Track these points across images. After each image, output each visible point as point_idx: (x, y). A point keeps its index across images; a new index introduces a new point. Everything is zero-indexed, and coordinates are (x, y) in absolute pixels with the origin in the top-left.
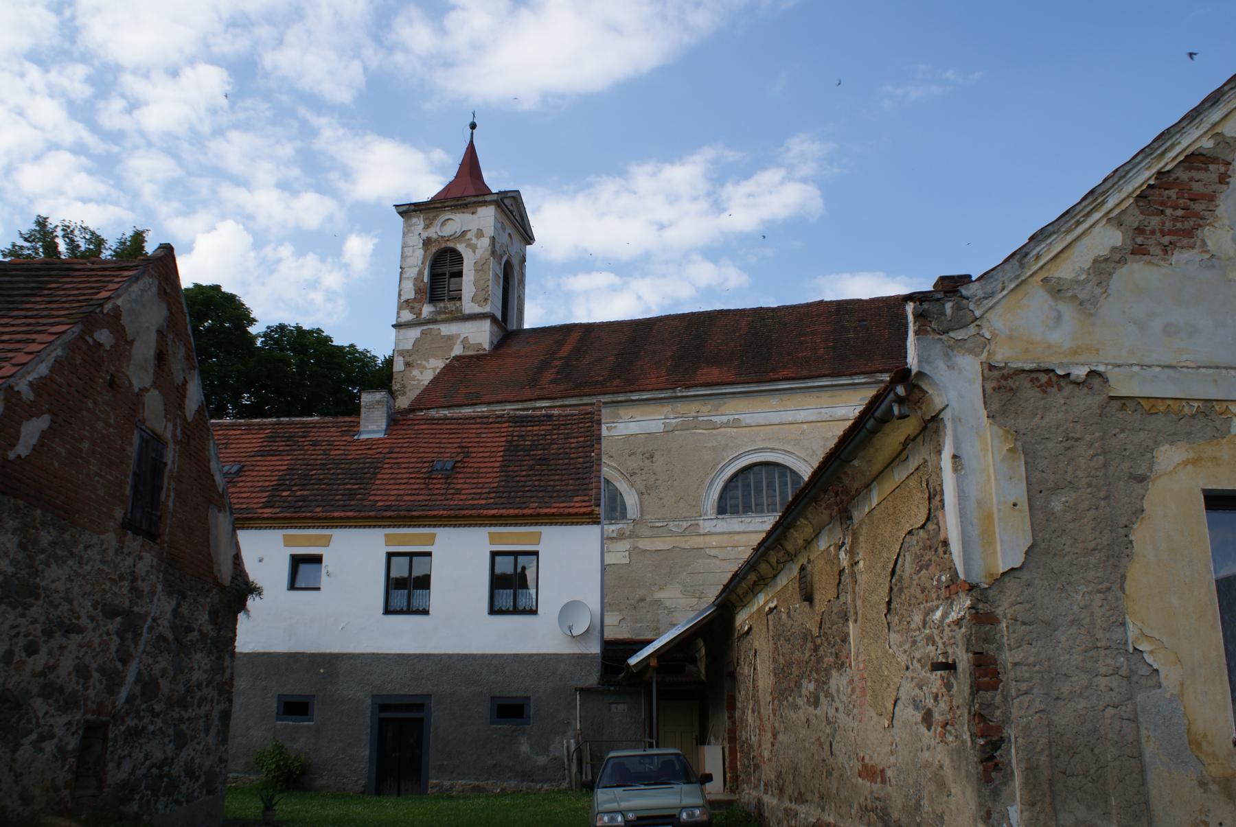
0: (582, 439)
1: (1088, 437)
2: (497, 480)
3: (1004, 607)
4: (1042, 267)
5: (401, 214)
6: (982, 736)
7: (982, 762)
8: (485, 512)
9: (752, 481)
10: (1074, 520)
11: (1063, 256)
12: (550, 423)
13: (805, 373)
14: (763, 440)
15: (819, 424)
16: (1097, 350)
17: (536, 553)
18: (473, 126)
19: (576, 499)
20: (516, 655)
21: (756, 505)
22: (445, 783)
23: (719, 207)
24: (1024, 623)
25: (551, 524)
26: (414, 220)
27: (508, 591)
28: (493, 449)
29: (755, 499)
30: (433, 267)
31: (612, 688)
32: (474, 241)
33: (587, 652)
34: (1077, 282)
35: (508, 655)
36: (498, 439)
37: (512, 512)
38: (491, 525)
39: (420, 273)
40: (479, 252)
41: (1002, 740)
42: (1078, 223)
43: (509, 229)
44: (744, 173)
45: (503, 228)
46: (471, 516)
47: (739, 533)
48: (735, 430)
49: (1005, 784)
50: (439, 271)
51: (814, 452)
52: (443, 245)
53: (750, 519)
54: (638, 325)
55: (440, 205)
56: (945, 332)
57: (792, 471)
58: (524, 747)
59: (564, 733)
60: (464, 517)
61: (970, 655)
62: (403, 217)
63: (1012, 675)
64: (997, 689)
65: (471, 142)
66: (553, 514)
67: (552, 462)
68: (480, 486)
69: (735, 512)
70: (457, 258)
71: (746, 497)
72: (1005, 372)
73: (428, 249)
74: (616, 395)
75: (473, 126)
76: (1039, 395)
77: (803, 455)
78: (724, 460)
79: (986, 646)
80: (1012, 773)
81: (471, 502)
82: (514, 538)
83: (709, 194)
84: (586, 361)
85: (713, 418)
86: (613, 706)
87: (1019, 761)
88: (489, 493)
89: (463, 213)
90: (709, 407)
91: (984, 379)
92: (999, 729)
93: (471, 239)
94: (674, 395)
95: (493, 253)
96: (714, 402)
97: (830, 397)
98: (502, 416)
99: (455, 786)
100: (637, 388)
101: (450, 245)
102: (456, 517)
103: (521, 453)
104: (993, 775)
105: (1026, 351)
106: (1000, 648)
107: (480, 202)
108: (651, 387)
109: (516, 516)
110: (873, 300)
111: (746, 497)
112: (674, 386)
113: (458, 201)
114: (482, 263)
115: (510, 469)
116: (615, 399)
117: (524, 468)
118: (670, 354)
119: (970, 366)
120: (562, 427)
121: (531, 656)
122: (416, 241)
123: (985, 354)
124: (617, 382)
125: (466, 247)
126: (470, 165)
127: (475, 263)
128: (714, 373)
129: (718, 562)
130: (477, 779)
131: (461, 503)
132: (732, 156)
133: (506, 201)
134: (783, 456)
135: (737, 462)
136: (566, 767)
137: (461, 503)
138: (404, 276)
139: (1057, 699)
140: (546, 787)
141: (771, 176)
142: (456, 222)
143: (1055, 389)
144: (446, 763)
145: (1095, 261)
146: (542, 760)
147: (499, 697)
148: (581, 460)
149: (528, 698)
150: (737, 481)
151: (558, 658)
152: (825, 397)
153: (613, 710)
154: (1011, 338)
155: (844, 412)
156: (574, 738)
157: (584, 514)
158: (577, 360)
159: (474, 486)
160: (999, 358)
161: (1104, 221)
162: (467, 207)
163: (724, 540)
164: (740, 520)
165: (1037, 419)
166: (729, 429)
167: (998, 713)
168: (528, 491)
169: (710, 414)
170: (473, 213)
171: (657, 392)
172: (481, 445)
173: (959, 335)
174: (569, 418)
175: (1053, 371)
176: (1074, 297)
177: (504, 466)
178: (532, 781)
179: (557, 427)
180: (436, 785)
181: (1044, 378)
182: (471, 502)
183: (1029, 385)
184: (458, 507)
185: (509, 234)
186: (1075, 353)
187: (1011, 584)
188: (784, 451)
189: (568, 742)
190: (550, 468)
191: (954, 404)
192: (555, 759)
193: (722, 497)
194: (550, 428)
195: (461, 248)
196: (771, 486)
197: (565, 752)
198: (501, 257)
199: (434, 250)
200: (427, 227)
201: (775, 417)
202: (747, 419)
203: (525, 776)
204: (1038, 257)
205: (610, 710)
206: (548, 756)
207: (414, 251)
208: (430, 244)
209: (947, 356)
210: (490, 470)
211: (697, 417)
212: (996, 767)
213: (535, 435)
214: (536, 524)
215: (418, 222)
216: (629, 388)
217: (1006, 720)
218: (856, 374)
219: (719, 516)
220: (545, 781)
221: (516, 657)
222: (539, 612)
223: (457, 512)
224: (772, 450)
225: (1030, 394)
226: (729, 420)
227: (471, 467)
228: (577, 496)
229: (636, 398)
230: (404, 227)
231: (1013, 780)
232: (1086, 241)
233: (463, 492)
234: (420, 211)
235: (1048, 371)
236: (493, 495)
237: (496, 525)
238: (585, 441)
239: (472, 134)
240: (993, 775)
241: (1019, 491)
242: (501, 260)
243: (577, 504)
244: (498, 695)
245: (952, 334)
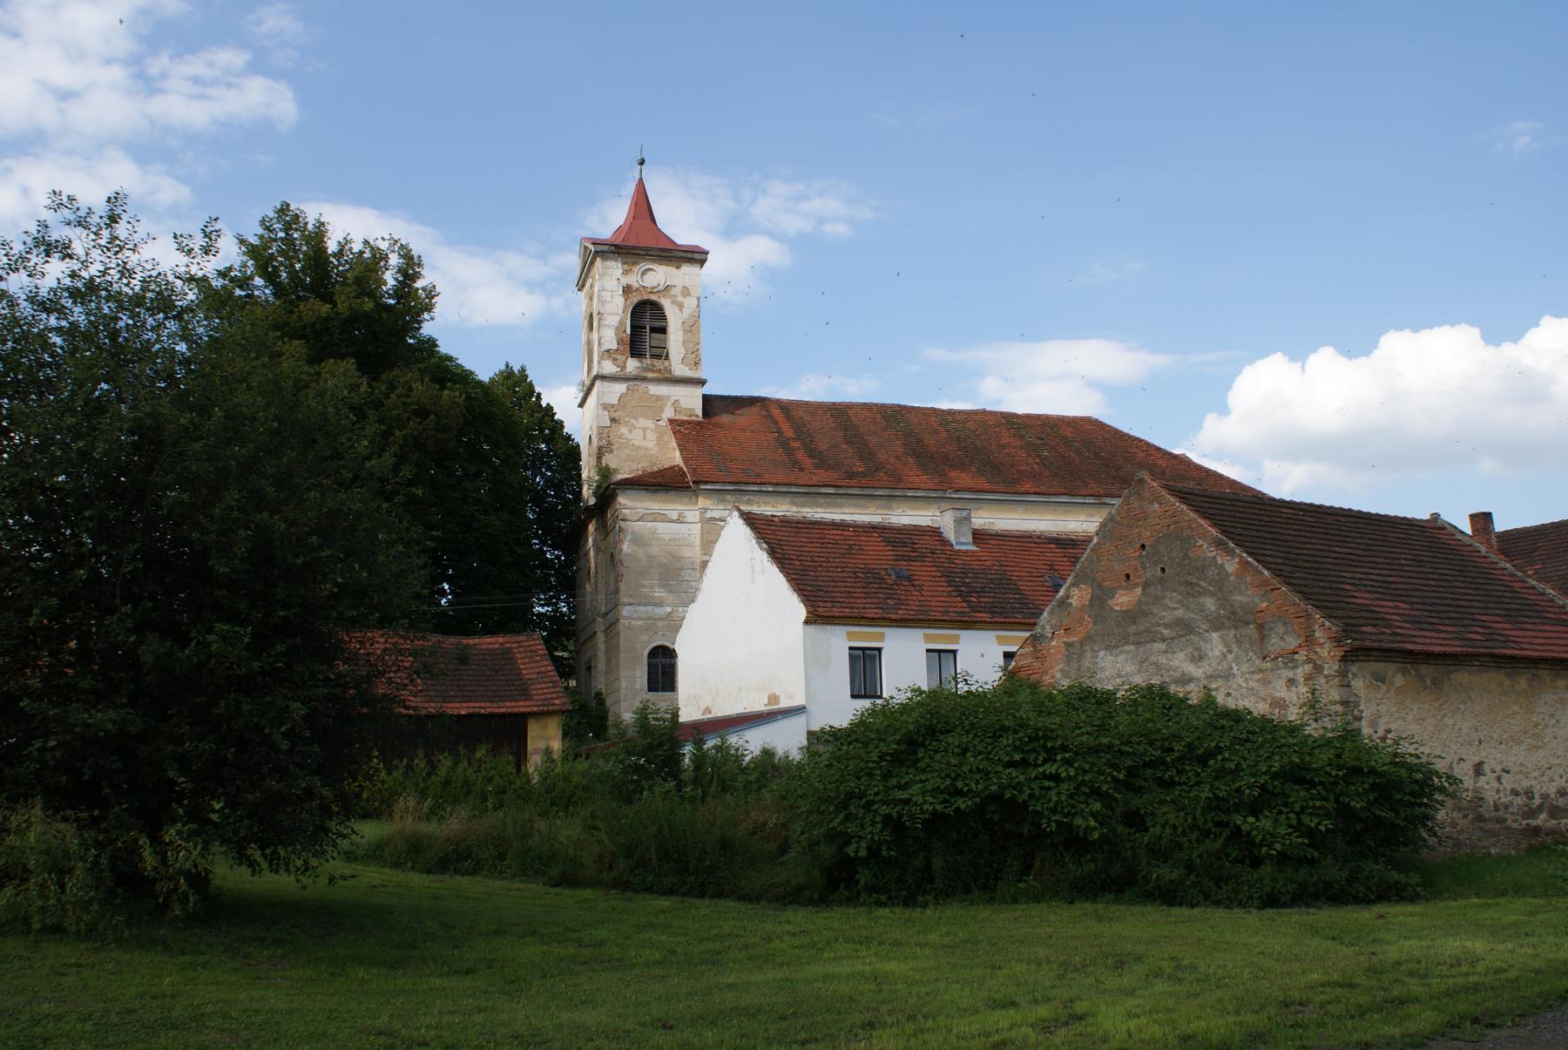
13: (1043, 489)
32: (680, 299)
52: (646, 297)
55: (643, 253)
65: (641, 179)
82: (865, 637)
101: (653, 297)
126: (642, 207)
138: (603, 322)
141: (230, 58)
170: (677, 268)
195: (666, 303)
199: (635, 300)
200: (626, 273)
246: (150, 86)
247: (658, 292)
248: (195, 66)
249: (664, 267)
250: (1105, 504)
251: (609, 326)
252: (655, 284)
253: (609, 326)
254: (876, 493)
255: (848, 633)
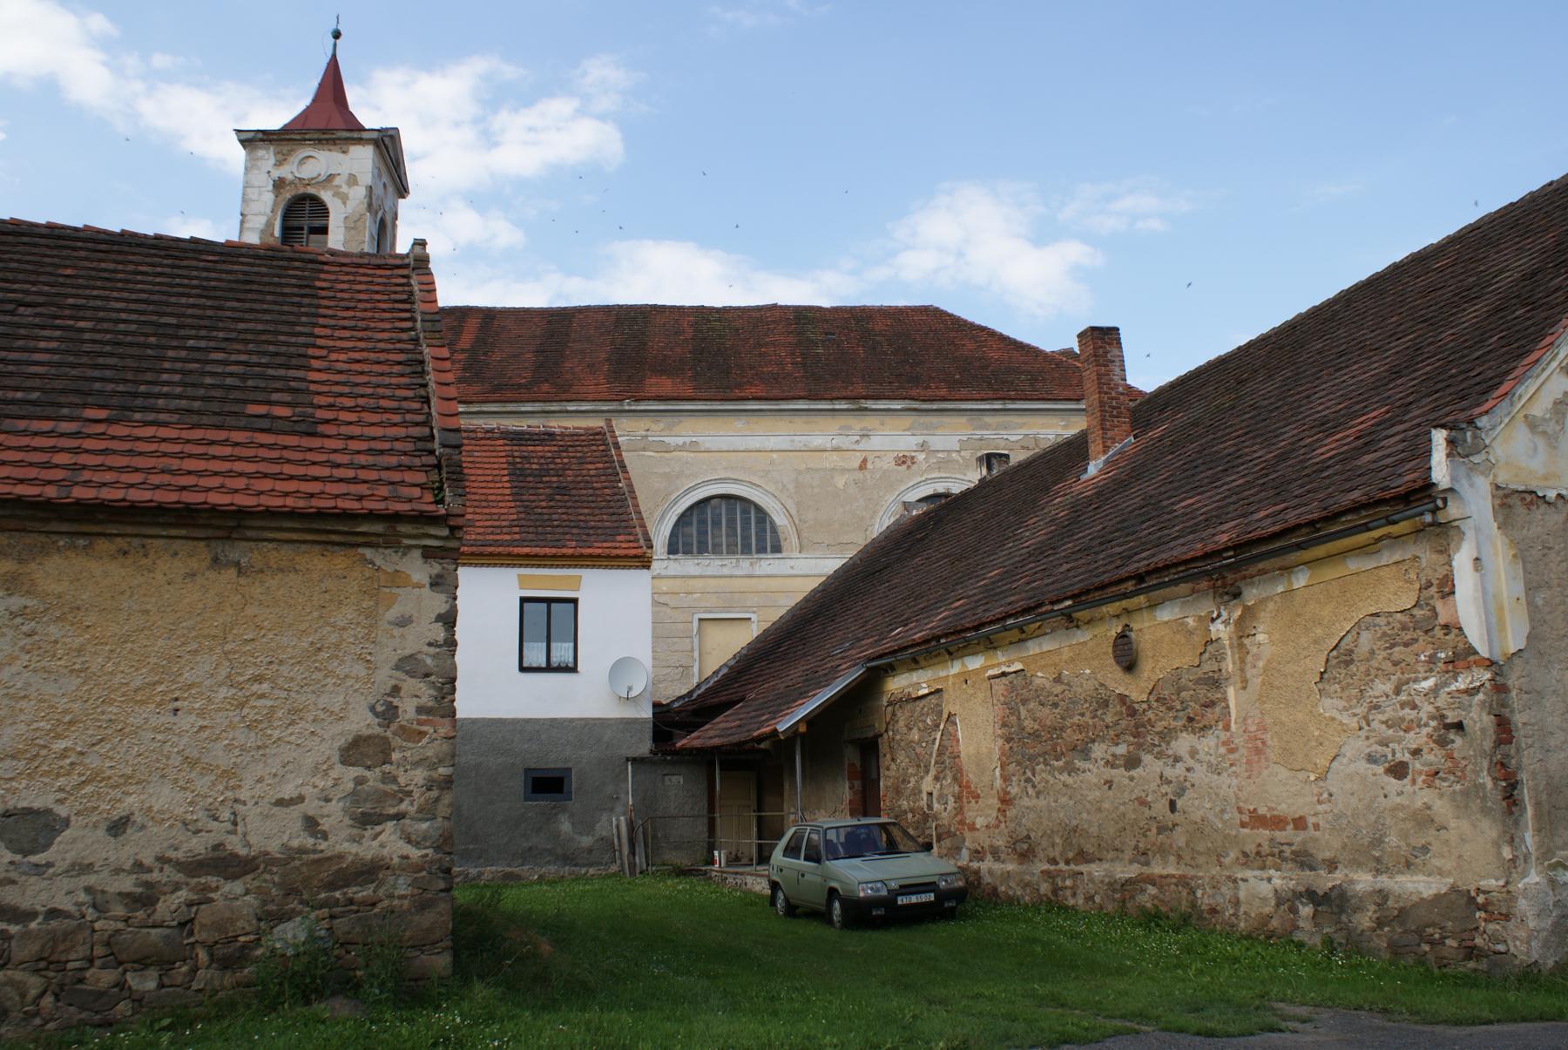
0: (601, 465)
1: (1557, 547)
2: (513, 511)
3: (1513, 680)
4: (1523, 406)
5: (242, 142)
6: (1505, 780)
7: (1504, 799)
8: (516, 550)
9: (709, 515)
10: (1550, 613)
11: (1535, 397)
12: (554, 443)
13: (775, 392)
14: (725, 468)
15: (790, 454)
16: (1559, 477)
17: (575, 601)
18: (337, 35)
19: (619, 538)
20: (553, 720)
21: (714, 546)
22: (471, 870)
23: (489, 140)
24: (1526, 693)
25: (593, 567)
26: (261, 153)
27: (540, 644)
28: (495, 472)
29: (713, 538)
30: (286, 216)
31: (669, 758)
32: (345, 189)
33: (638, 716)
34: (1545, 420)
35: (545, 719)
36: (496, 460)
37: (548, 551)
38: (521, 566)
39: (269, 224)
40: (351, 205)
41: (1517, 782)
42: (1544, 370)
43: (385, 179)
44: (525, 98)
45: (380, 176)
46: (499, 554)
47: (694, 577)
48: (692, 455)
49: (1521, 815)
50: (295, 223)
51: (784, 486)
52: (302, 191)
53: (708, 561)
54: (552, 315)
55: (298, 137)
56: (1467, 456)
57: (759, 509)
58: (565, 826)
59: (612, 810)
60: (491, 555)
61: (1493, 717)
62: (244, 147)
63: (1522, 733)
64: (1511, 743)
65: (334, 56)
66: (599, 556)
67: (573, 492)
68: (496, 517)
69: (688, 552)
70: (321, 209)
71: (702, 533)
72: (1505, 491)
73: (281, 194)
74: (548, 404)
75: (337, 35)
76: (1526, 511)
77: (771, 488)
78: (678, 490)
79: (1503, 710)
80: (1525, 808)
81: (492, 537)
82: (549, 581)
83: (476, 121)
84: (497, 357)
85: (667, 439)
86: (667, 778)
87: (1530, 798)
88: (511, 526)
89: (330, 150)
90: (662, 425)
91: (1493, 496)
92: (1514, 774)
93: (341, 187)
94: (620, 408)
95: (370, 205)
96: (668, 420)
97: (806, 423)
98: (491, 431)
99: (483, 874)
100: (574, 397)
101: (311, 190)
102: (481, 555)
103: (530, 479)
104: (1514, 809)
105: (1516, 475)
106: (1512, 712)
107: (353, 139)
108: (591, 397)
109: (554, 556)
110: (835, 310)
111: (702, 533)
112: (621, 397)
113: (324, 134)
114: (356, 219)
115: (525, 498)
116: (547, 409)
117: (541, 497)
118: (603, 356)
119: (1483, 484)
120: (570, 449)
121: (572, 720)
122: (264, 182)
123: (1491, 476)
124: (545, 387)
125: (333, 196)
126: (332, 86)
127: (346, 218)
128: (666, 385)
129: (669, 610)
130: (509, 865)
131: (479, 537)
132: (510, 72)
133: (385, 139)
134: (750, 490)
135: (693, 493)
136: (616, 848)
137: (479, 537)
138: (246, 225)
139: (1548, 751)
140: (591, 871)
141: (560, 107)
142: (316, 164)
143: (1535, 507)
144: (471, 847)
145: (1555, 403)
146: (586, 841)
147: (535, 769)
148: (607, 491)
149: (569, 770)
150: (691, 515)
151: (603, 723)
152: (799, 422)
153: (667, 783)
154: (1507, 463)
155: (820, 441)
156: (624, 814)
157: (636, 556)
158: (485, 354)
159: (488, 517)
160: (1500, 480)
161: (1558, 370)
162: (335, 144)
163: (677, 585)
164: (696, 561)
165: (1525, 531)
166: (685, 454)
167: (1513, 761)
168: (558, 526)
169: (662, 434)
170: (344, 152)
171: (600, 403)
172: (477, 465)
173: (1476, 459)
174: (575, 438)
175: (1535, 492)
176: (1544, 433)
177: (517, 494)
178: (575, 865)
179: (565, 448)
180: (460, 874)
181: (1528, 497)
182: (492, 537)
183: (1520, 503)
184: (479, 543)
185: (384, 185)
186: (1546, 478)
187: (1517, 661)
188: (750, 482)
189: (618, 820)
190: (574, 499)
191: (1475, 516)
192: (602, 839)
193: (673, 534)
194: (556, 449)
195: (326, 196)
196: (731, 523)
197: (615, 831)
198: (377, 213)
199: (288, 196)
200: (279, 164)
201: (740, 443)
202: (707, 442)
203: (568, 859)
204: (1520, 396)
205: (663, 781)
206: (593, 835)
207: (260, 194)
208: (283, 188)
209: (1469, 476)
210: (499, 498)
211: (647, 436)
212: (1515, 803)
213: (542, 457)
214: (576, 566)
215: (267, 156)
216: (564, 396)
217: (1519, 767)
218: (838, 398)
219: (671, 557)
220: (591, 865)
221: (553, 722)
222: (579, 669)
223: (482, 549)
224: (736, 481)
225: (1520, 510)
226: (685, 443)
227: (474, 494)
228: (620, 535)
229: (574, 408)
230: (246, 161)
231: (1526, 812)
232: (1548, 385)
233: (477, 524)
234: (270, 141)
235: (1532, 492)
236: (517, 529)
237: (527, 566)
238: (604, 468)
239: (335, 45)
240: (1514, 809)
241: (1519, 589)
242: (376, 216)
243: (621, 545)
244: (533, 766)
245: (1471, 458)
246: (489, 140)
247: (318, 182)
248: (529, 117)
249: (326, 153)
250: (866, 409)
251: (252, 229)
252: (315, 175)
253: (252, 229)
254: (523, 409)
255: (519, 575)
